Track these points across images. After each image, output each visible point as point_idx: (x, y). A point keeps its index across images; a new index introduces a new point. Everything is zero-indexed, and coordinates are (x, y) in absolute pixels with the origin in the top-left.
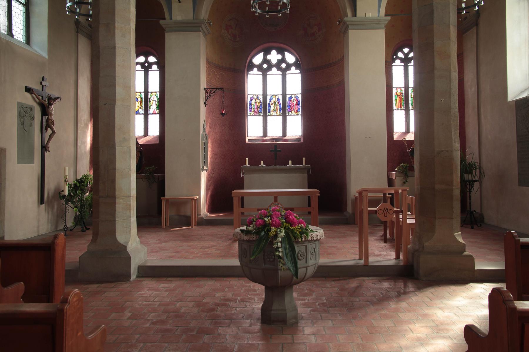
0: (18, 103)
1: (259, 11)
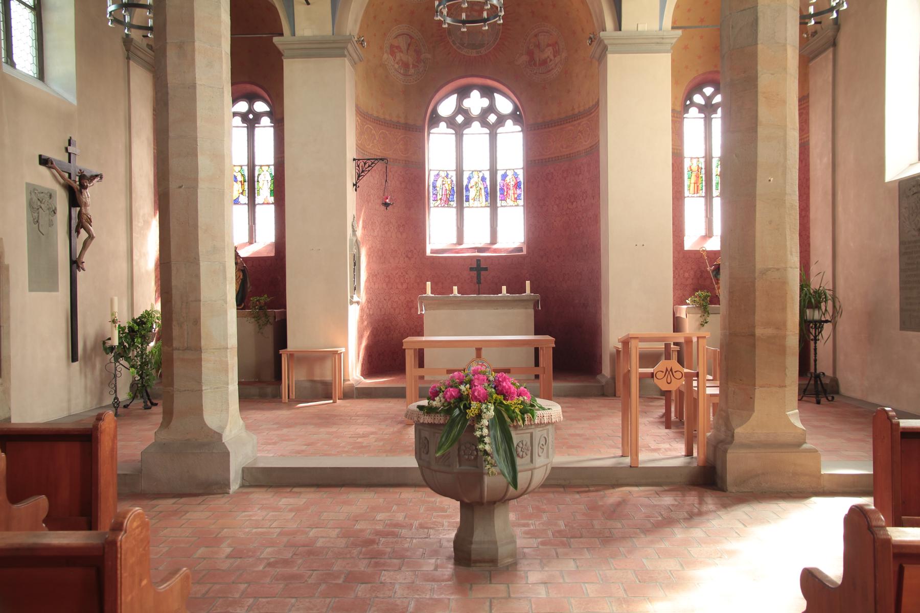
1: (449, 20)
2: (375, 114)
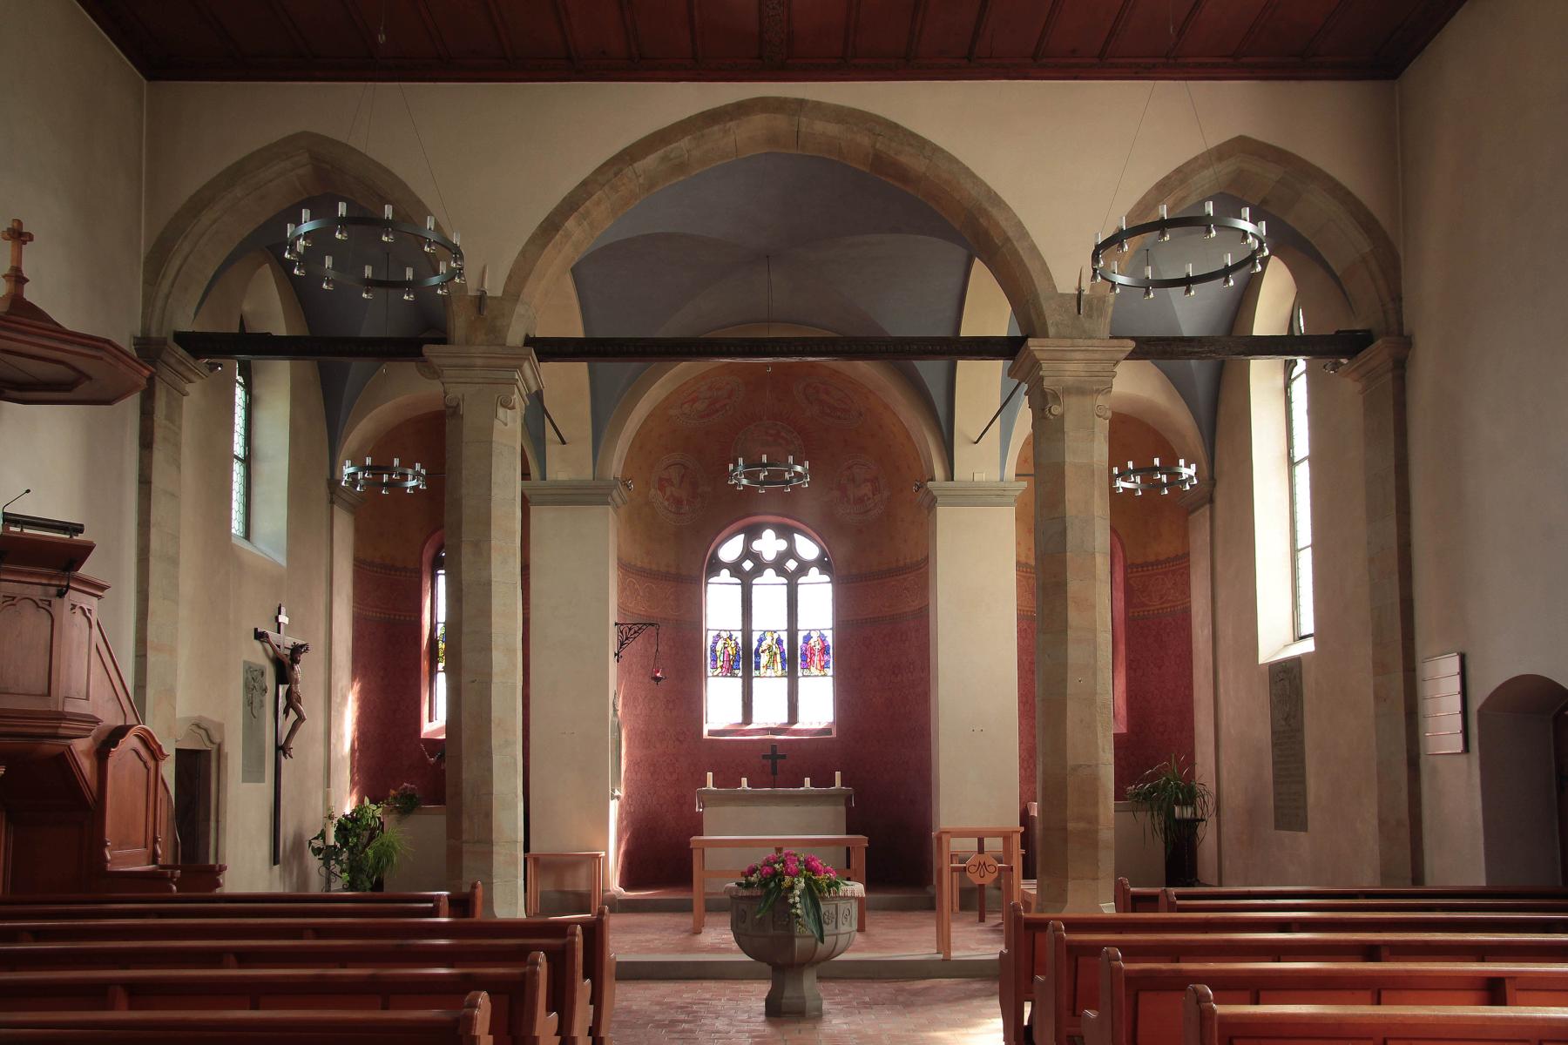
0: (245, 662)
1: (745, 482)
2: (639, 564)
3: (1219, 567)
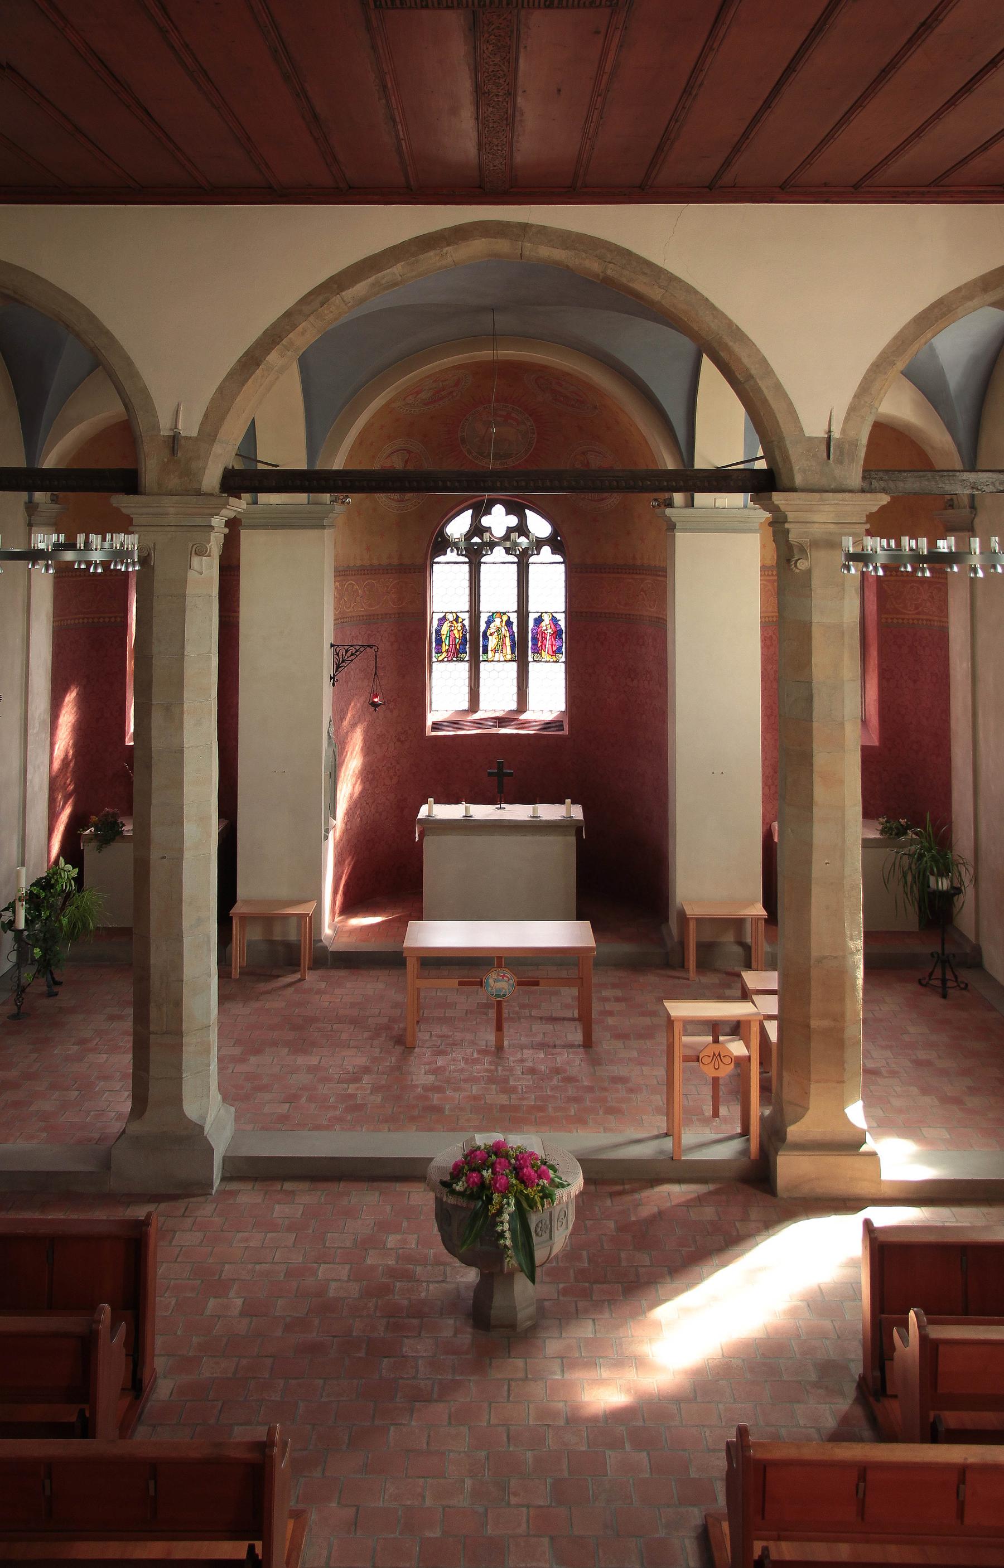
3: (979, 603)
